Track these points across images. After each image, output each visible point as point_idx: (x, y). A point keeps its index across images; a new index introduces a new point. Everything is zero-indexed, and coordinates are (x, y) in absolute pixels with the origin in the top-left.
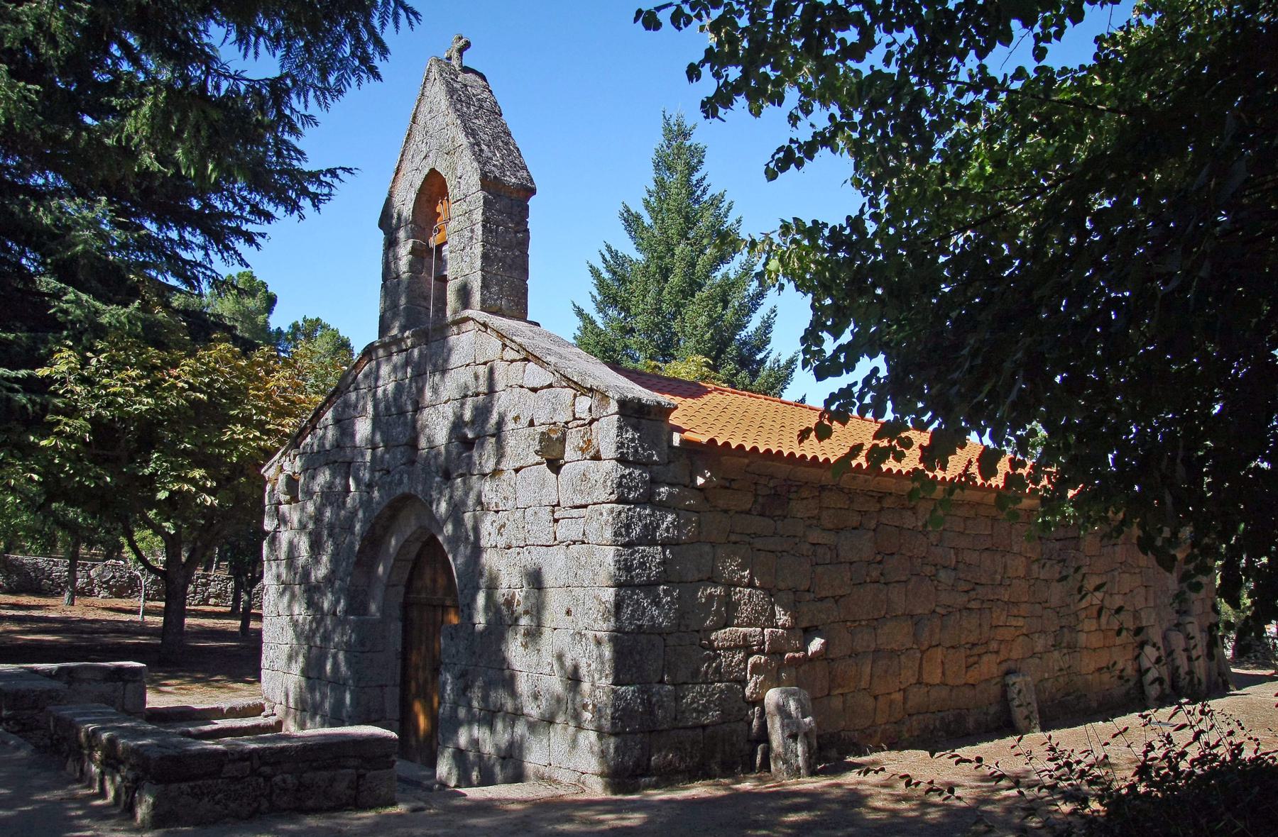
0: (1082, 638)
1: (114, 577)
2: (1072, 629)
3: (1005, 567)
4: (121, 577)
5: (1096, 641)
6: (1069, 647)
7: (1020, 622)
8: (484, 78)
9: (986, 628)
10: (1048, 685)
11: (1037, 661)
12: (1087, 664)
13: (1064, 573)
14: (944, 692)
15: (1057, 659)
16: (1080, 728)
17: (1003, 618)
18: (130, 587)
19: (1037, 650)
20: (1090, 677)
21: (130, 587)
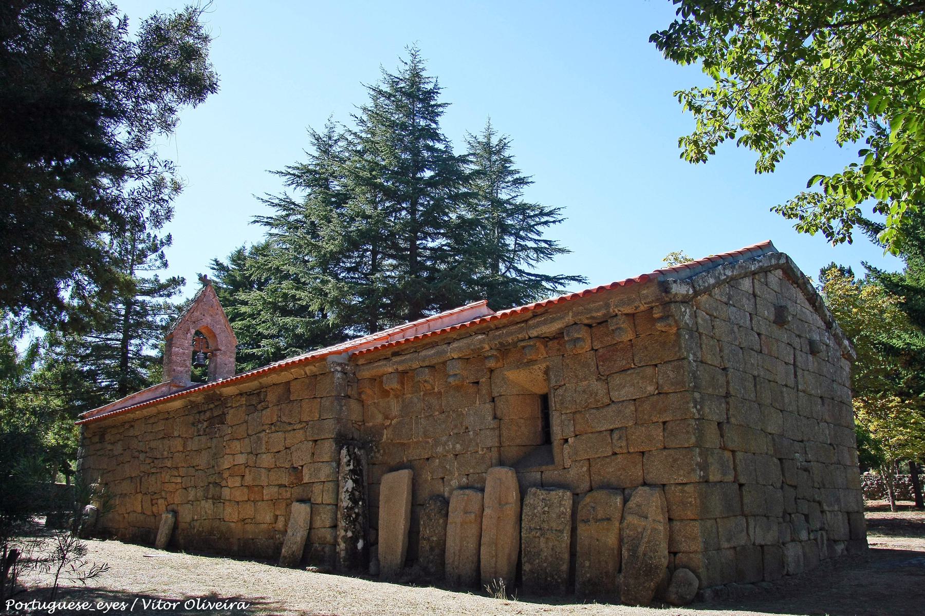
0: (226, 493)
1: (866, 485)
2: (216, 484)
3: (169, 447)
4: (872, 484)
5: (239, 495)
6: (213, 498)
7: (179, 480)
8: (815, 177)
9: (159, 483)
10: (197, 524)
11: (190, 506)
12: (230, 513)
13: (209, 445)
14: (142, 517)
15: (208, 505)
16: (365, 581)
17: (168, 477)
18: (879, 491)
19: (190, 498)
20: (232, 524)
21: (879, 491)
